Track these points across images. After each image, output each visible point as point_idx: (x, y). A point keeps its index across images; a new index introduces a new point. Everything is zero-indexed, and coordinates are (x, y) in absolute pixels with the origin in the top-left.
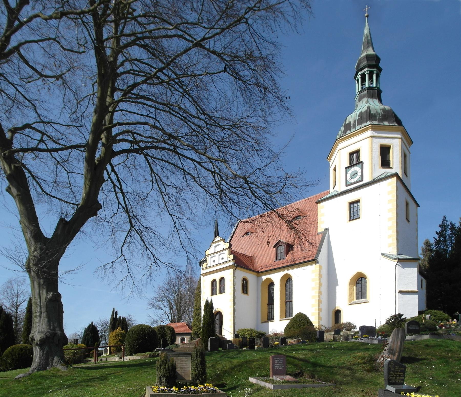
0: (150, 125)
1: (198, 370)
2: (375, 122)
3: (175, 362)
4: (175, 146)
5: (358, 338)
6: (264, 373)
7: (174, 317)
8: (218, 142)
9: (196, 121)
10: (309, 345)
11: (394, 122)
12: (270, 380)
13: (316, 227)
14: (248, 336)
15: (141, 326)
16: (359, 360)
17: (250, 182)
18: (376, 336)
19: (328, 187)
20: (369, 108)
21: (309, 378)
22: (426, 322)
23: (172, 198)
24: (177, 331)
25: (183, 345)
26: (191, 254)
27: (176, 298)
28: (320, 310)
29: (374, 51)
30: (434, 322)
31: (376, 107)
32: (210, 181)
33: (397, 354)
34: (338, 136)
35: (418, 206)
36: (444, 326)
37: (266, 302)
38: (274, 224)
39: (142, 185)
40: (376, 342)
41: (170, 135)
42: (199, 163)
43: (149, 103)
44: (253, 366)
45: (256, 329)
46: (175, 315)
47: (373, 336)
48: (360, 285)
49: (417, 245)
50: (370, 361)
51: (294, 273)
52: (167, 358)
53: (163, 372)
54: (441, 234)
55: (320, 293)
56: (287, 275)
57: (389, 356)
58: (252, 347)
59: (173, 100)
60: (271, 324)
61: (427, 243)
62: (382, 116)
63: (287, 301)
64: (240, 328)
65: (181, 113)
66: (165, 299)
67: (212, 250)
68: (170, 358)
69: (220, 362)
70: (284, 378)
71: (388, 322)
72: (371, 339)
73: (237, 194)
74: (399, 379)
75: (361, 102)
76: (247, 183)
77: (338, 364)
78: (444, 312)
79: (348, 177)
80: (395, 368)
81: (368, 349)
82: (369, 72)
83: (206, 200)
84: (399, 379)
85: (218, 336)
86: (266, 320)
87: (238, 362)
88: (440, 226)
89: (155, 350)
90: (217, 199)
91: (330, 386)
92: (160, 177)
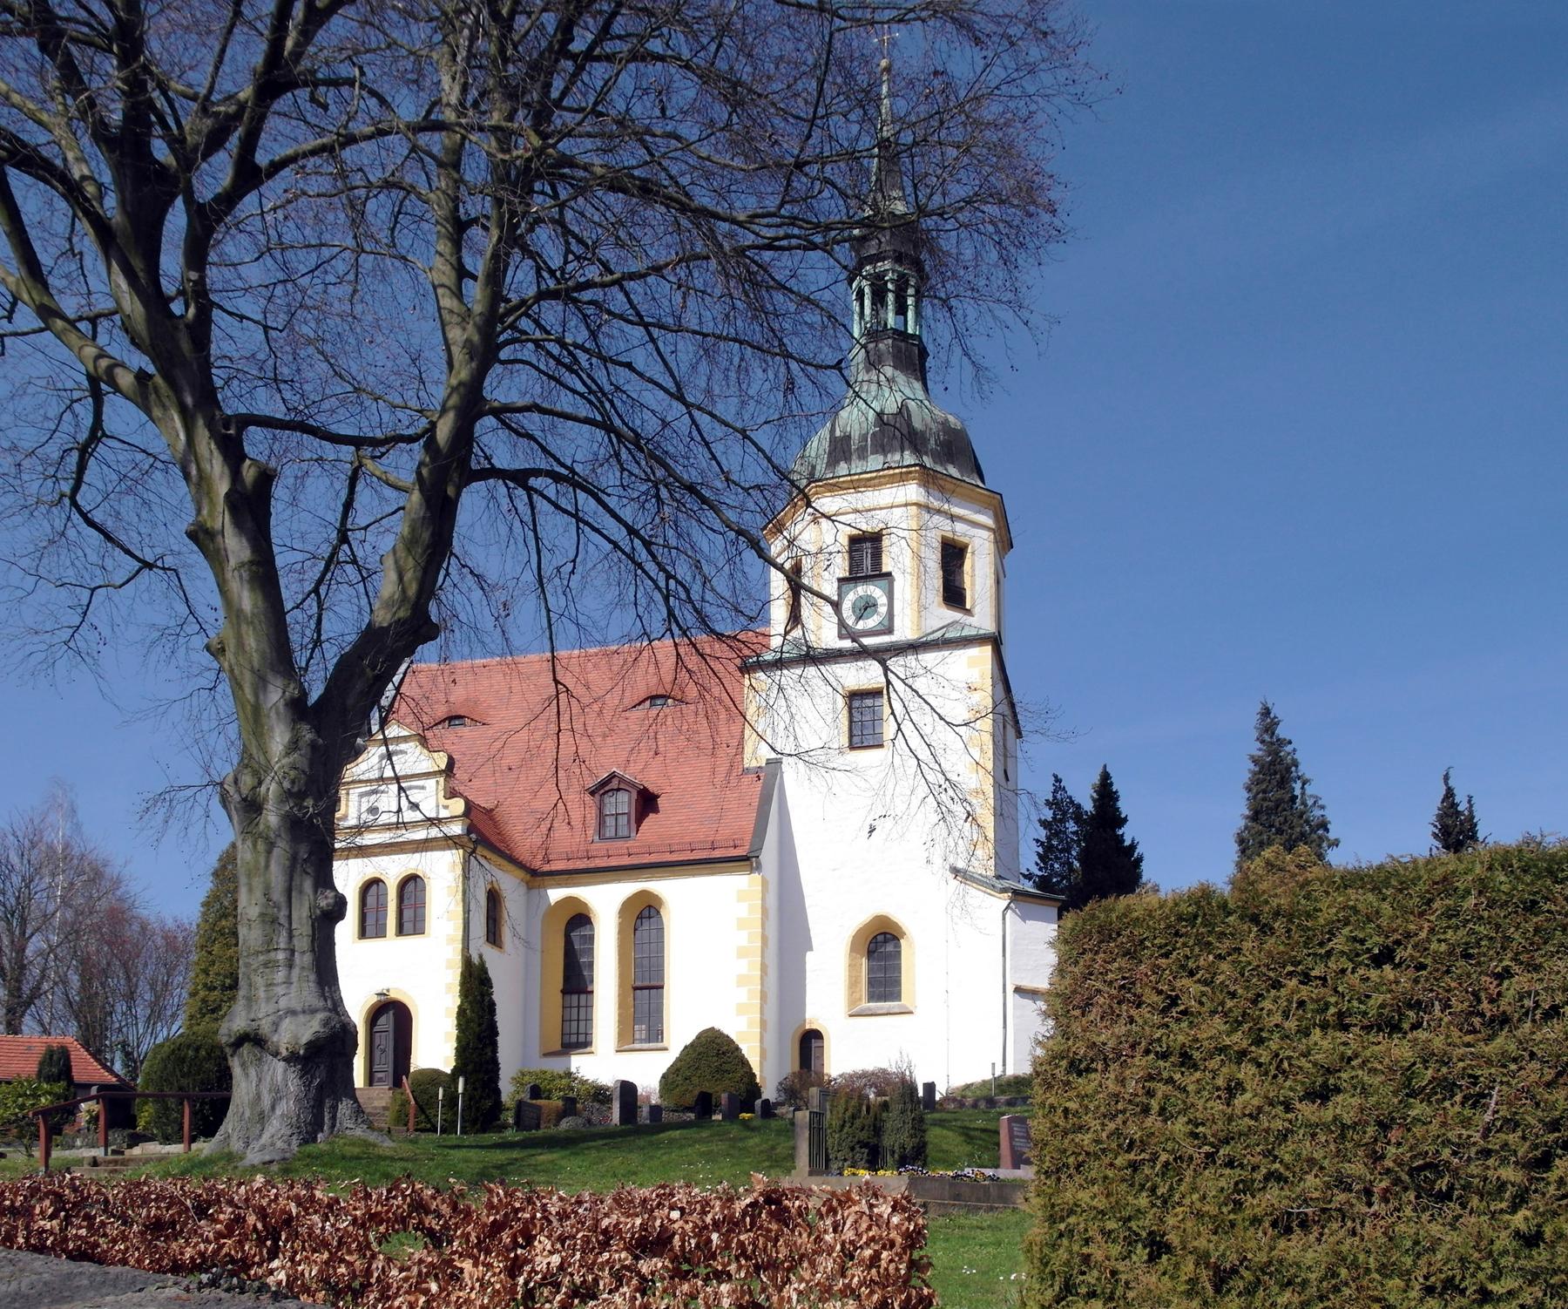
63: (639, 984)
86: (558, 1047)
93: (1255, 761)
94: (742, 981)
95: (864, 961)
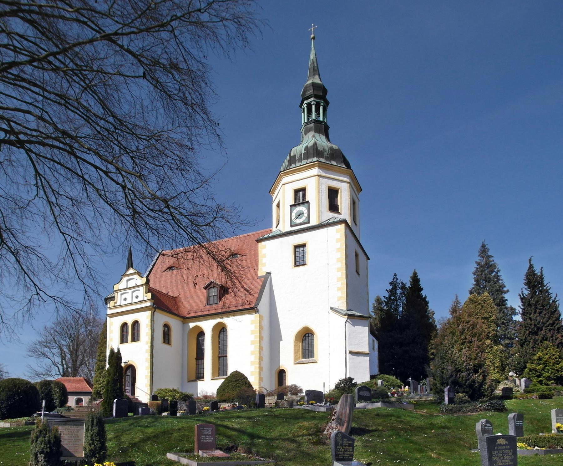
0: (35, 115)
1: (93, 444)
2: (322, 160)
3: (59, 433)
4: (71, 147)
5: (304, 404)
6: (187, 446)
7: (67, 369)
8: (132, 152)
9: (102, 123)
10: (246, 411)
11: (342, 163)
12: (194, 456)
13: (256, 269)
14: (170, 398)
15: (14, 380)
16: (304, 432)
17: (171, 206)
18: (323, 403)
19: (271, 226)
20: (315, 143)
21: (245, 453)
22: (378, 388)
23: (65, 212)
24: (69, 389)
25: (77, 409)
26: (91, 288)
27: (71, 344)
28: (261, 369)
29: (321, 81)
30: (386, 388)
31: (323, 143)
32: (120, 198)
33: (345, 425)
34: (282, 169)
35: (368, 259)
36: (395, 393)
37: (194, 355)
38: (202, 262)
39: (22, 188)
40: (323, 409)
41: (64, 133)
42: (106, 173)
43: (37, 90)
44: (173, 437)
45: (180, 390)
46: (69, 367)
47: (321, 402)
48: (307, 341)
49: (368, 301)
50: (317, 432)
51: (229, 321)
52: (48, 427)
53: (40, 446)
54: (392, 292)
55: (261, 348)
56: (220, 324)
57: (337, 426)
58: (174, 413)
59: (71, 92)
60: (200, 383)
61: (378, 300)
62: (330, 154)
63: (220, 355)
64: (159, 388)
65: (81, 110)
66: (54, 345)
67: (122, 285)
68: (54, 426)
69: (128, 433)
70: (213, 453)
71: (337, 387)
72: (318, 405)
73: (154, 218)
74: (347, 454)
75: (307, 135)
76: (168, 207)
77: (280, 436)
78: (397, 378)
79: (293, 218)
80: (343, 441)
81: (314, 418)
82: (315, 103)
83: (113, 220)
84: (347, 454)
85: (129, 398)
87: (152, 433)
88: (391, 283)
89: (35, 415)
90: (129, 221)
91: (269, 463)
92: (48, 182)
93: (478, 264)
94: (252, 353)
95: (301, 344)
